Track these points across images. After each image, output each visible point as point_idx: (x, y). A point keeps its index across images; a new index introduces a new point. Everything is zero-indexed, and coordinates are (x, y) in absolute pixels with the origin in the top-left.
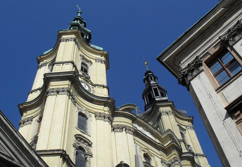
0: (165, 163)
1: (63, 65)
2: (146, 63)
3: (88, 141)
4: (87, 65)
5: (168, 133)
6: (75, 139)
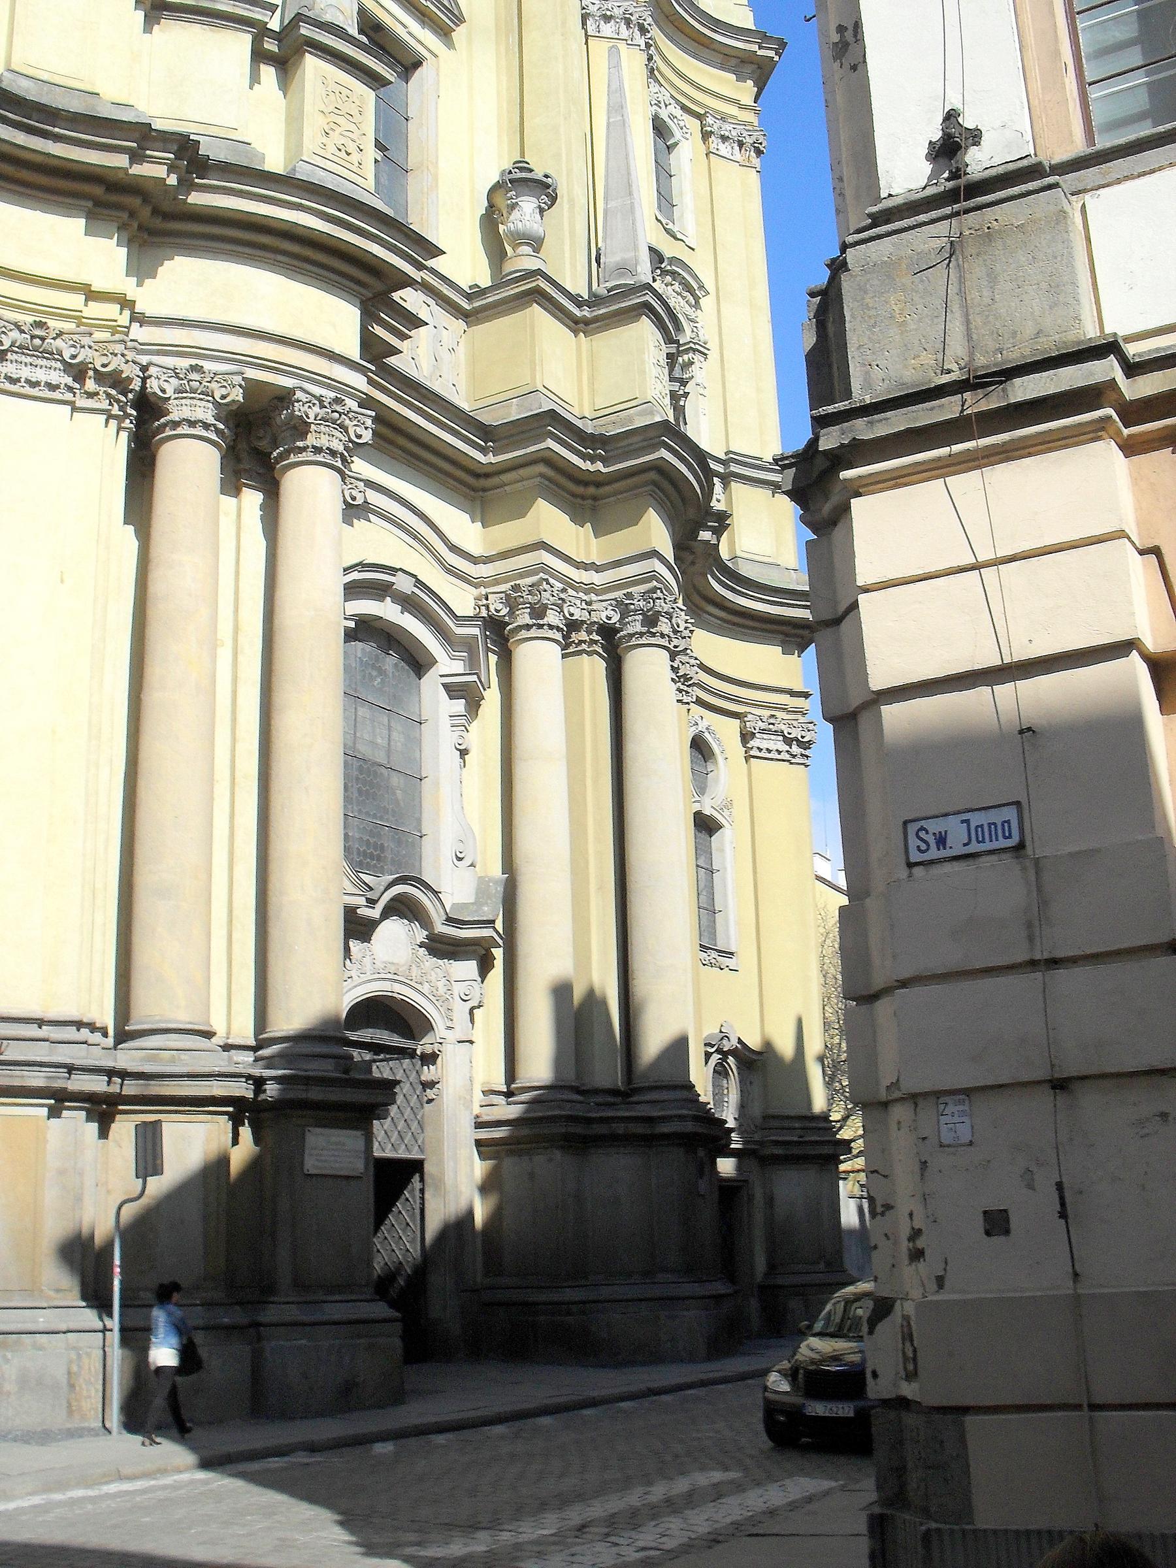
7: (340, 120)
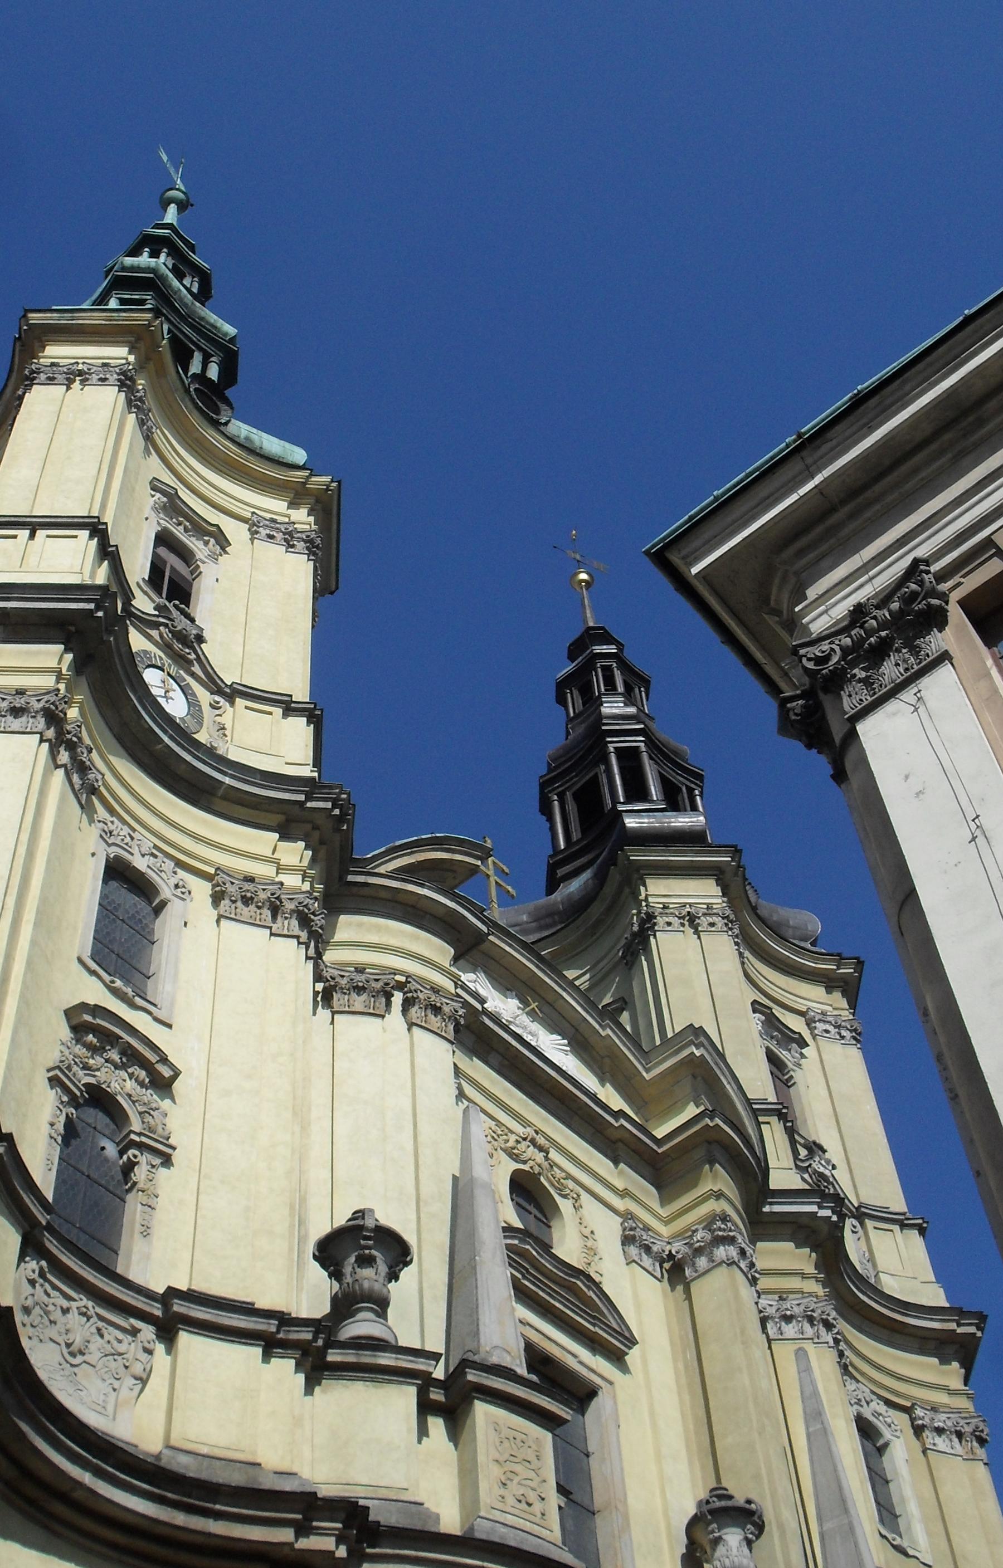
0: (648, 1249)
1: (32, 536)
2: (583, 576)
3: (153, 1058)
4: (192, 554)
5: (685, 1053)
6: (65, 1033)
7: (518, 1468)
